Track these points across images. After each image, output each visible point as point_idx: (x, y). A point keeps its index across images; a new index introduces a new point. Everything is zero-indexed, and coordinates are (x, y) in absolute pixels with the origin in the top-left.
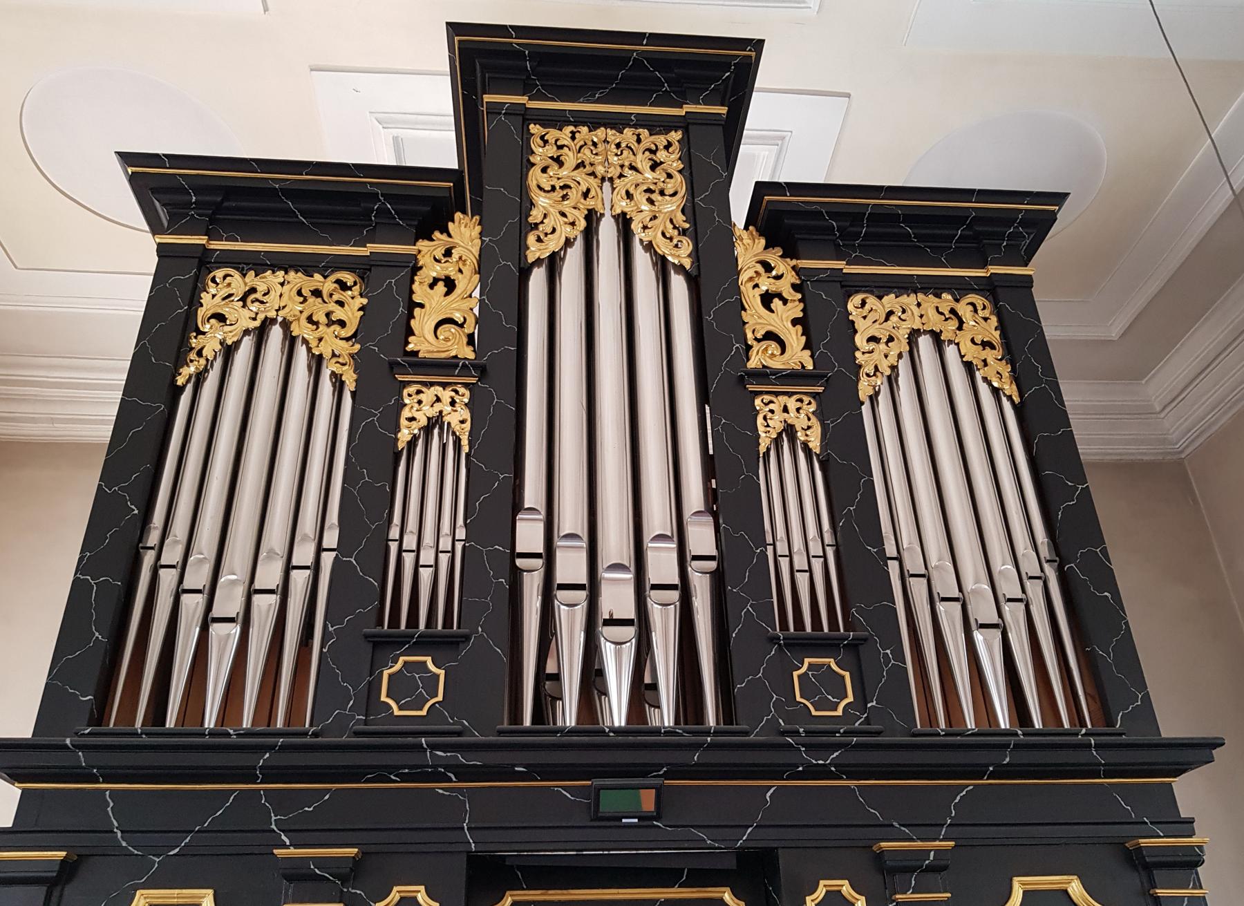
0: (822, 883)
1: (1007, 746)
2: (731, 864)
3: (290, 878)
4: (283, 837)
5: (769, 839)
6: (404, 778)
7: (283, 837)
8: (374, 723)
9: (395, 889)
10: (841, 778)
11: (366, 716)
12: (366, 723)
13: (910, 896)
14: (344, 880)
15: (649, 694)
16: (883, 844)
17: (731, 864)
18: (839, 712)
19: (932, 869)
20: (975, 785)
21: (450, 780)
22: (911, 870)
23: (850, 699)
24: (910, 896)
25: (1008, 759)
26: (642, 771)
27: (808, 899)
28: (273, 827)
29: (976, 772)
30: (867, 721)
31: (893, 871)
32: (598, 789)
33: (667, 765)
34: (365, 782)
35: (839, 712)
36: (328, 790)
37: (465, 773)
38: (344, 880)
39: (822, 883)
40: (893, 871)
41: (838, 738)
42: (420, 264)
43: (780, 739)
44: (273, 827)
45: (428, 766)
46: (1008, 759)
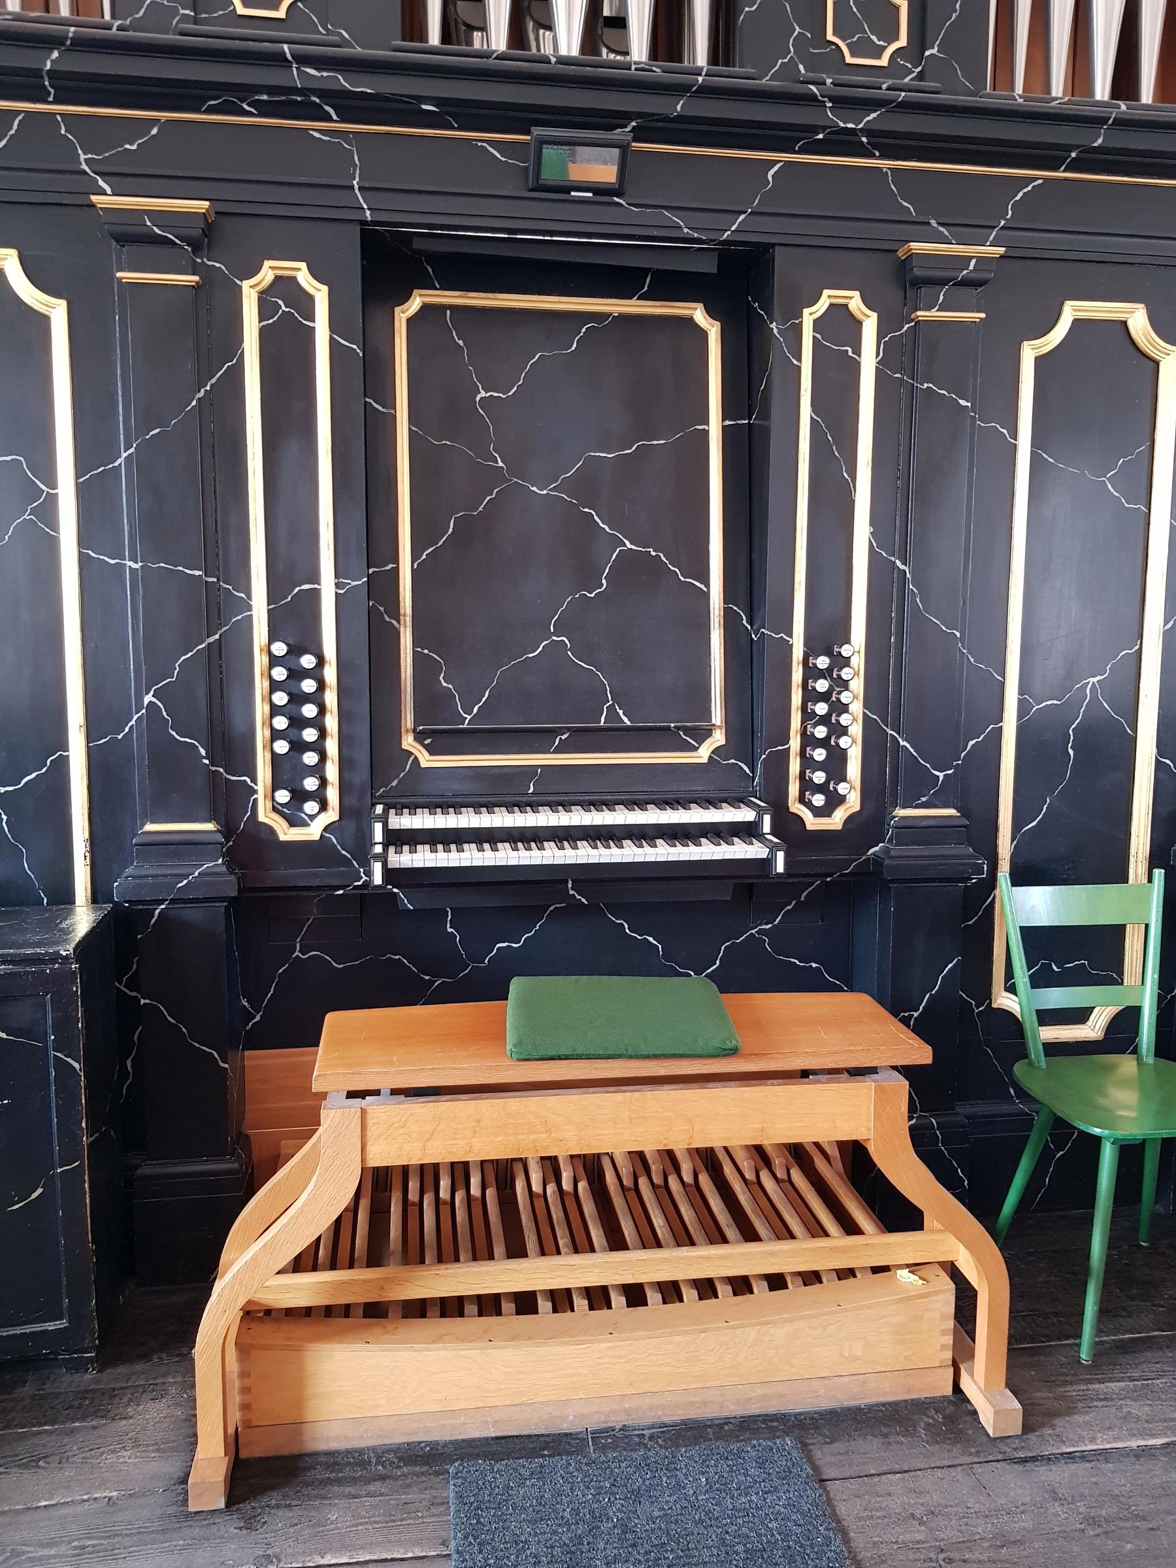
0: (826, 292)
1: (1104, 120)
2: (709, 266)
3: (123, 239)
4: (101, 183)
5: (767, 231)
6: (264, 110)
7: (101, 183)
8: (205, 22)
9: (267, 264)
10: (872, 156)
11: (194, 9)
12: (196, 21)
13: (934, 314)
14: (197, 248)
15: (609, 34)
16: (913, 245)
17: (709, 266)
18: (884, 61)
19: (966, 283)
20: (1046, 179)
21: (329, 119)
22: (942, 282)
23: (903, 42)
24: (934, 314)
25: (1100, 141)
26: (607, 120)
27: (806, 311)
28: (84, 167)
29: (1048, 157)
30: (921, 76)
31: (918, 283)
32: (542, 142)
33: (639, 115)
34: (207, 112)
35: (884, 61)
36: (155, 121)
37: (353, 107)
38: (197, 248)
39: (826, 292)
40: (918, 283)
41: (883, 93)
42: (316, 1087)
43: (800, 88)
44: (84, 167)
45: (294, 90)
46: (1100, 141)
